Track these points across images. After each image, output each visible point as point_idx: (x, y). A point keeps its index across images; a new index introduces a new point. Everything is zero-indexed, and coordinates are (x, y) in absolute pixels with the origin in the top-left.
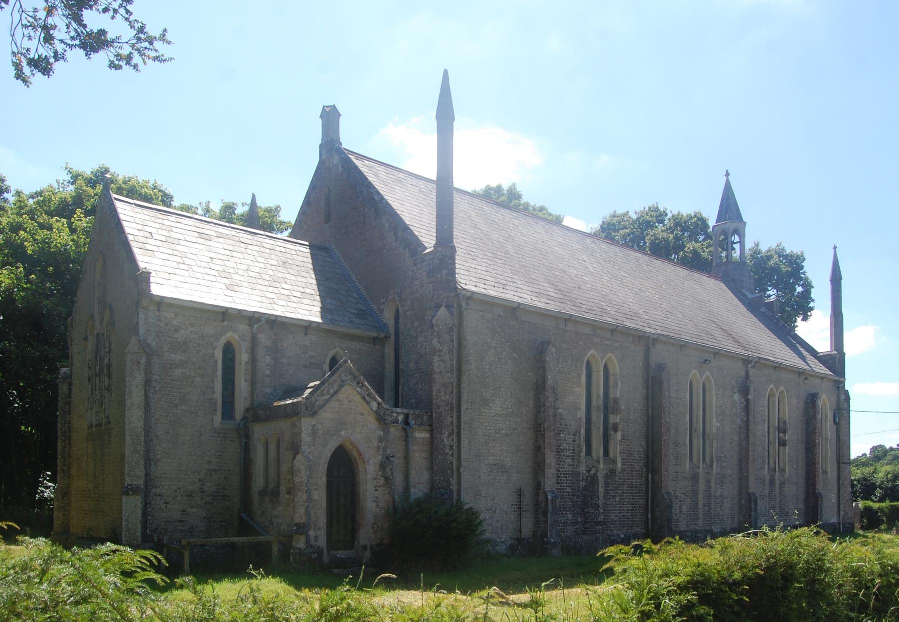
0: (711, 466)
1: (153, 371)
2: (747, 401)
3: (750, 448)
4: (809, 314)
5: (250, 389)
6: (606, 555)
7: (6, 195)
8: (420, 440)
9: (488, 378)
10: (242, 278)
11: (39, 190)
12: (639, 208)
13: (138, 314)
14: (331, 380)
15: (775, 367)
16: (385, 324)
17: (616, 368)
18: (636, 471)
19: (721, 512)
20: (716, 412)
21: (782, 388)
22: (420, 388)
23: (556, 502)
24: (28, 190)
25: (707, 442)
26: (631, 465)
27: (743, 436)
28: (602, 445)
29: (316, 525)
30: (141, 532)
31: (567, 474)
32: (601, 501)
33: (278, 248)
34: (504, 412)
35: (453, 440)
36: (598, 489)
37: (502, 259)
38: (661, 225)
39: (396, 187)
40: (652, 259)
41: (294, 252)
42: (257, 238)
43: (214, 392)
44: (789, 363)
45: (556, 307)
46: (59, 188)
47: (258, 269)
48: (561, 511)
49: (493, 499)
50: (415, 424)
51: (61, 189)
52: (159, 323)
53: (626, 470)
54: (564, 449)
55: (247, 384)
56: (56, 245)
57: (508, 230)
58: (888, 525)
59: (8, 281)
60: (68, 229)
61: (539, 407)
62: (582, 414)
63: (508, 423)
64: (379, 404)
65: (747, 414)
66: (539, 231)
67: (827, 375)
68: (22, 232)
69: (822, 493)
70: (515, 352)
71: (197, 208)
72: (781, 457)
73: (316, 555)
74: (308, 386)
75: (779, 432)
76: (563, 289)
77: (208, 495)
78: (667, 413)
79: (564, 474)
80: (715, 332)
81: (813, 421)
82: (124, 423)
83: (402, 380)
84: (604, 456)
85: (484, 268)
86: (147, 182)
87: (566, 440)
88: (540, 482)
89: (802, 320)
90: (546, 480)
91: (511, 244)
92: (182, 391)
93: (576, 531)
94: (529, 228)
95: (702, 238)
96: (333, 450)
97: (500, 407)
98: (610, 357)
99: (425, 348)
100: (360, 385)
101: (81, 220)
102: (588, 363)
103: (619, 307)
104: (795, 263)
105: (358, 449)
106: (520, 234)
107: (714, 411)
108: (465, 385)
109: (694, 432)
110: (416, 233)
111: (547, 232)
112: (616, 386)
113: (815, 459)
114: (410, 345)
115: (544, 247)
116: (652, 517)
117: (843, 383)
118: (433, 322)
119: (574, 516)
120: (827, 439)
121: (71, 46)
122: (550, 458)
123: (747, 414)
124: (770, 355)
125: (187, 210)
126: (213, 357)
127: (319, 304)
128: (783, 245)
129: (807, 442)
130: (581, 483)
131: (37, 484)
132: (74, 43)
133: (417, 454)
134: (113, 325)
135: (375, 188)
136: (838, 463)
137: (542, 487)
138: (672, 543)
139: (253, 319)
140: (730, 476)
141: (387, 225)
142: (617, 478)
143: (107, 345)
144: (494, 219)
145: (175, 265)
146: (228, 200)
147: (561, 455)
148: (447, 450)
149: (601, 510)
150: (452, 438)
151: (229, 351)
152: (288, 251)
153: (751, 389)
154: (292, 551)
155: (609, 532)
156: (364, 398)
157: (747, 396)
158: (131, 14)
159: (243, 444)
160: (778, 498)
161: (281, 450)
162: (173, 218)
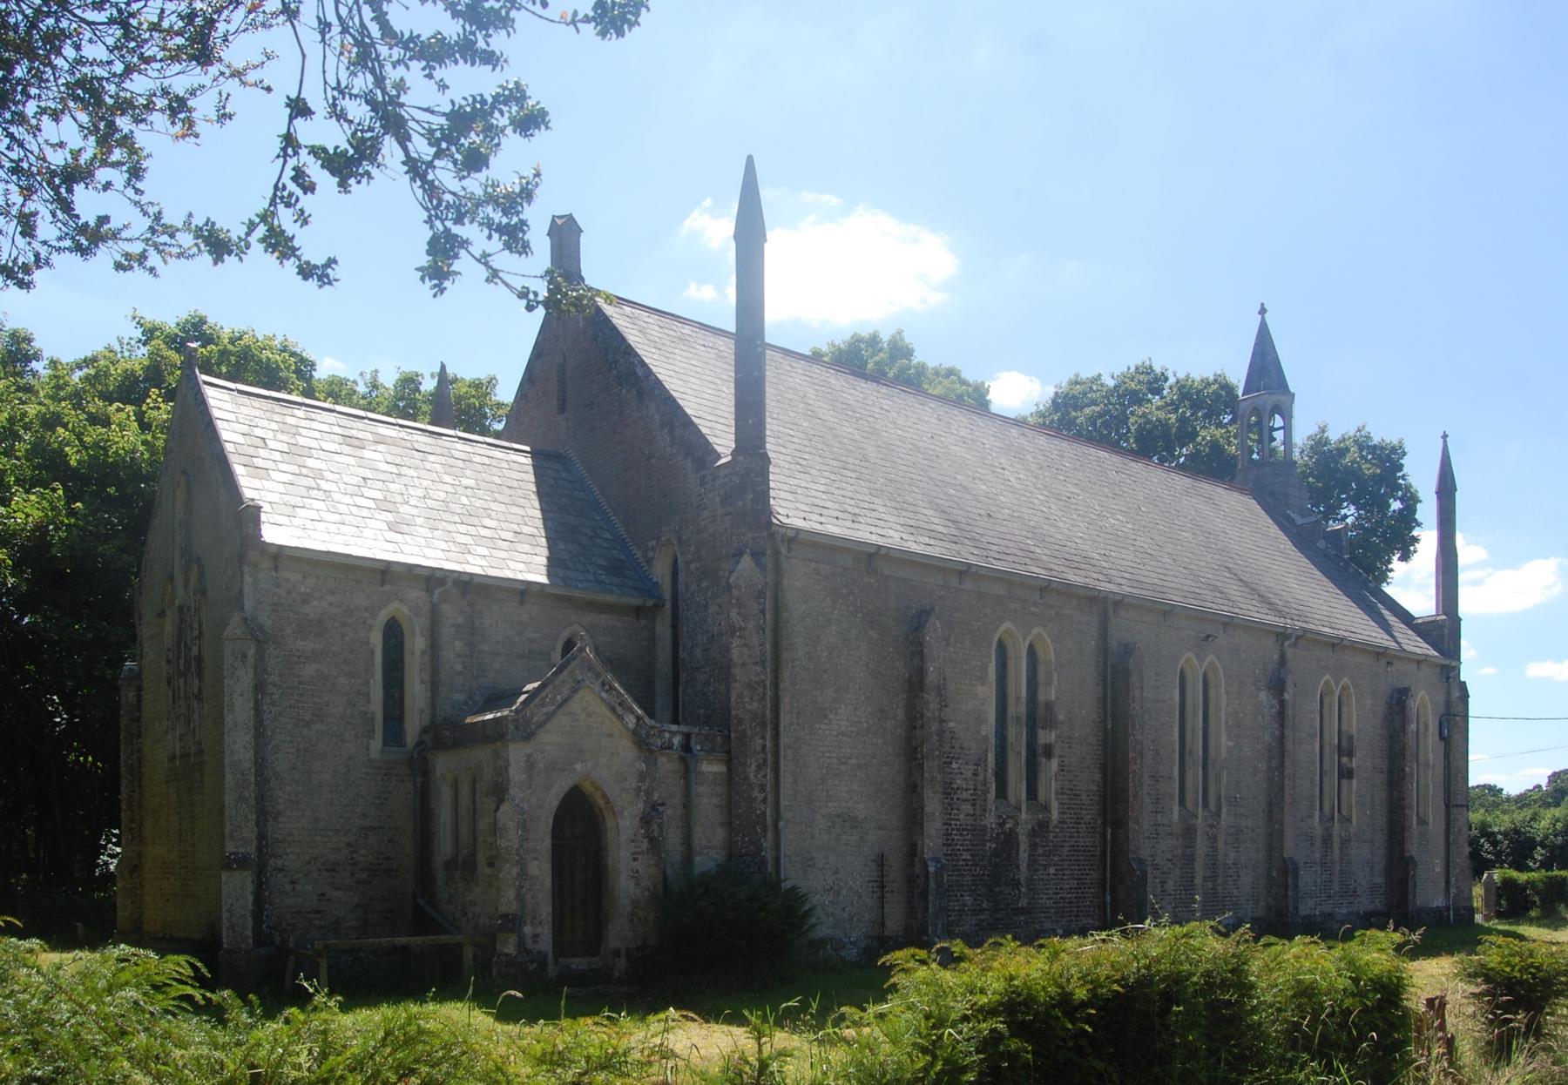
0: (1218, 814)
1: (269, 669)
2: (1282, 703)
3: (1286, 782)
4: (1412, 548)
5: (429, 694)
6: (888, 964)
7: (34, 365)
8: (711, 777)
9: (825, 672)
10: (415, 511)
11: (89, 355)
12: (1120, 369)
13: (242, 576)
14: (558, 681)
15: (1333, 645)
16: (657, 583)
17: (1048, 652)
18: (1085, 823)
19: (1236, 891)
20: (1226, 722)
21: (1346, 680)
22: (712, 689)
23: (942, 877)
24: (68, 356)
25: (1212, 774)
26: (1075, 813)
27: (1274, 763)
28: (1025, 782)
29: (534, 917)
30: (253, 929)
31: (963, 830)
32: (1023, 873)
33: (477, 459)
34: (854, 729)
35: (765, 776)
36: (1017, 854)
37: (854, 471)
38: (1157, 397)
39: (677, 351)
40: (1126, 461)
41: (505, 465)
42: (444, 442)
43: (369, 701)
44: (1360, 637)
45: (943, 551)
46: (122, 352)
47: (442, 496)
48: (953, 891)
49: (836, 872)
50: (701, 750)
51: (126, 354)
52: (277, 590)
53: (1066, 823)
54: (958, 789)
55: (423, 686)
56: (116, 452)
57: (871, 419)
58: (1542, 911)
59: (37, 514)
60: (136, 424)
61: (914, 718)
62: (989, 728)
63: (860, 746)
64: (639, 718)
65: (1282, 726)
66: (926, 418)
67: (1427, 656)
68: (60, 430)
69: (1416, 858)
70: (872, 628)
71: (355, 382)
72: (1344, 795)
73: (535, 965)
74: (525, 690)
75: (1340, 753)
76: (960, 519)
77: (362, 870)
78: (1137, 727)
79: (958, 830)
80: (1228, 586)
81: (1401, 735)
82: (223, 752)
83: (683, 677)
84: (1027, 799)
85: (822, 488)
86: (270, 339)
87: (961, 774)
88: (915, 844)
89: (1401, 559)
90: (926, 841)
91: (874, 443)
92: (316, 699)
93: (978, 924)
94: (910, 414)
95: (1227, 418)
96: (562, 795)
97: (847, 720)
98: (1039, 634)
99: (720, 624)
100: (607, 687)
101: (159, 408)
102: (1001, 644)
103: (1057, 547)
104: (1389, 460)
105: (603, 792)
106: (891, 426)
107: (1223, 721)
108: (785, 684)
109: (1187, 758)
110: (704, 430)
111: (940, 420)
112: (1050, 682)
113: (1404, 799)
114: (697, 619)
115: (933, 447)
116: (1113, 900)
117: (1457, 669)
118: (730, 581)
119: (975, 900)
120: (1427, 765)
121: (59, 250)
122: (933, 804)
123: (1282, 726)
124: (1326, 624)
125: (338, 392)
126: (368, 643)
127: (545, 552)
128: (1367, 429)
129: (1391, 772)
130: (988, 844)
131: (98, 850)
132: (62, 244)
133: (705, 800)
134: (204, 592)
135: (639, 356)
136: (1447, 806)
137: (919, 851)
138: (1001, 945)
139: (432, 579)
140: (1253, 831)
141: (657, 417)
142: (1052, 835)
143: (196, 625)
144: (847, 401)
145: (304, 492)
146: (409, 368)
147: (952, 799)
148: (756, 793)
149: (1023, 890)
150: (763, 773)
151: (394, 634)
152: (494, 462)
153: (1289, 684)
154: (495, 959)
155: (1038, 926)
156: (613, 710)
157: (1282, 695)
158: (142, 192)
159: (419, 785)
160: (1338, 867)
161: (478, 795)
162: (300, 413)
